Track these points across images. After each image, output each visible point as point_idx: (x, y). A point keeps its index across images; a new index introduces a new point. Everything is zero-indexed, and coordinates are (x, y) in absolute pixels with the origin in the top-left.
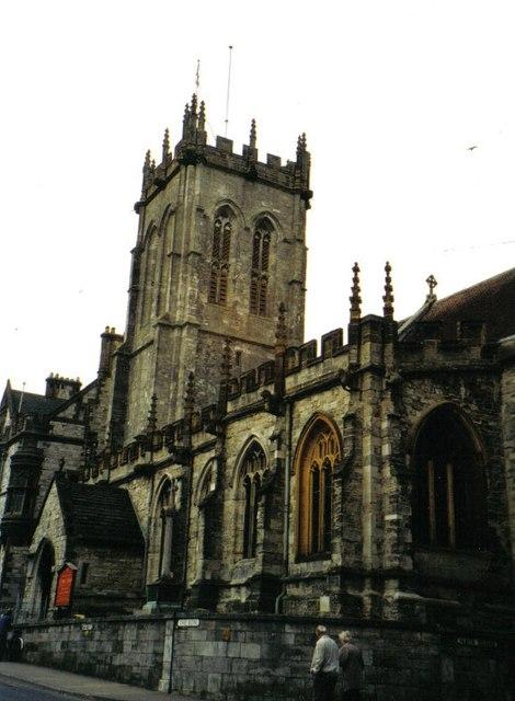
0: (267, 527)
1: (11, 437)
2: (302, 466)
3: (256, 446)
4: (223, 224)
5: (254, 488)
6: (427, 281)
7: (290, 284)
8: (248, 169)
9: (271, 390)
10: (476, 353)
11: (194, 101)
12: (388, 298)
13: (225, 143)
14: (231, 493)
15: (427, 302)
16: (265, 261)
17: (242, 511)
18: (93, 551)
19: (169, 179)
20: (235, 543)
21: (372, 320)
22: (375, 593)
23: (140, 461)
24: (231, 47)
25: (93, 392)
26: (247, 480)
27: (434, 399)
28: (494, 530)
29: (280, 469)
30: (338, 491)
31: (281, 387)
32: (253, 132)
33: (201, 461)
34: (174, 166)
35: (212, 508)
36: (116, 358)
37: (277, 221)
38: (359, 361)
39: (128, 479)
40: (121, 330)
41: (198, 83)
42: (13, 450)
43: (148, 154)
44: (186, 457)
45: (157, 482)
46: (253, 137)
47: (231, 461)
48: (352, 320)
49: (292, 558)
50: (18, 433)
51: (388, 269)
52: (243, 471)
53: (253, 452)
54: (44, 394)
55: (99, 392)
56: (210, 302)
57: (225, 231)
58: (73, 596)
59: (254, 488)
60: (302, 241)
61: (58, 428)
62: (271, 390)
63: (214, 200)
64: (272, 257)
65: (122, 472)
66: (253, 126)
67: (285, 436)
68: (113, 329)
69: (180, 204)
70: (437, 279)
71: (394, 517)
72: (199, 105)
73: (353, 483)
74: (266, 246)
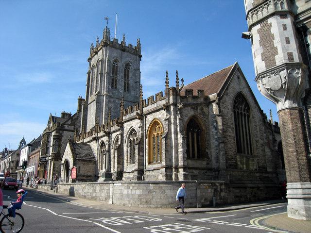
0: (139, 155)
3: (133, 130)
8: (123, 48)
9: (139, 112)
13: (116, 40)
14: (125, 145)
19: (99, 51)
23: (94, 136)
24: (106, 19)
26: (131, 141)
27: (192, 113)
28: (207, 153)
33: (114, 136)
34: (100, 47)
35: (120, 149)
38: (169, 102)
39: (90, 141)
40: (84, 97)
42: (53, 134)
44: (109, 134)
45: (99, 142)
46: (124, 39)
47: (125, 135)
51: (177, 73)
52: (129, 137)
53: (132, 132)
58: (77, 176)
61: (66, 127)
62: (139, 112)
64: (131, 75)
74: (128, 71)
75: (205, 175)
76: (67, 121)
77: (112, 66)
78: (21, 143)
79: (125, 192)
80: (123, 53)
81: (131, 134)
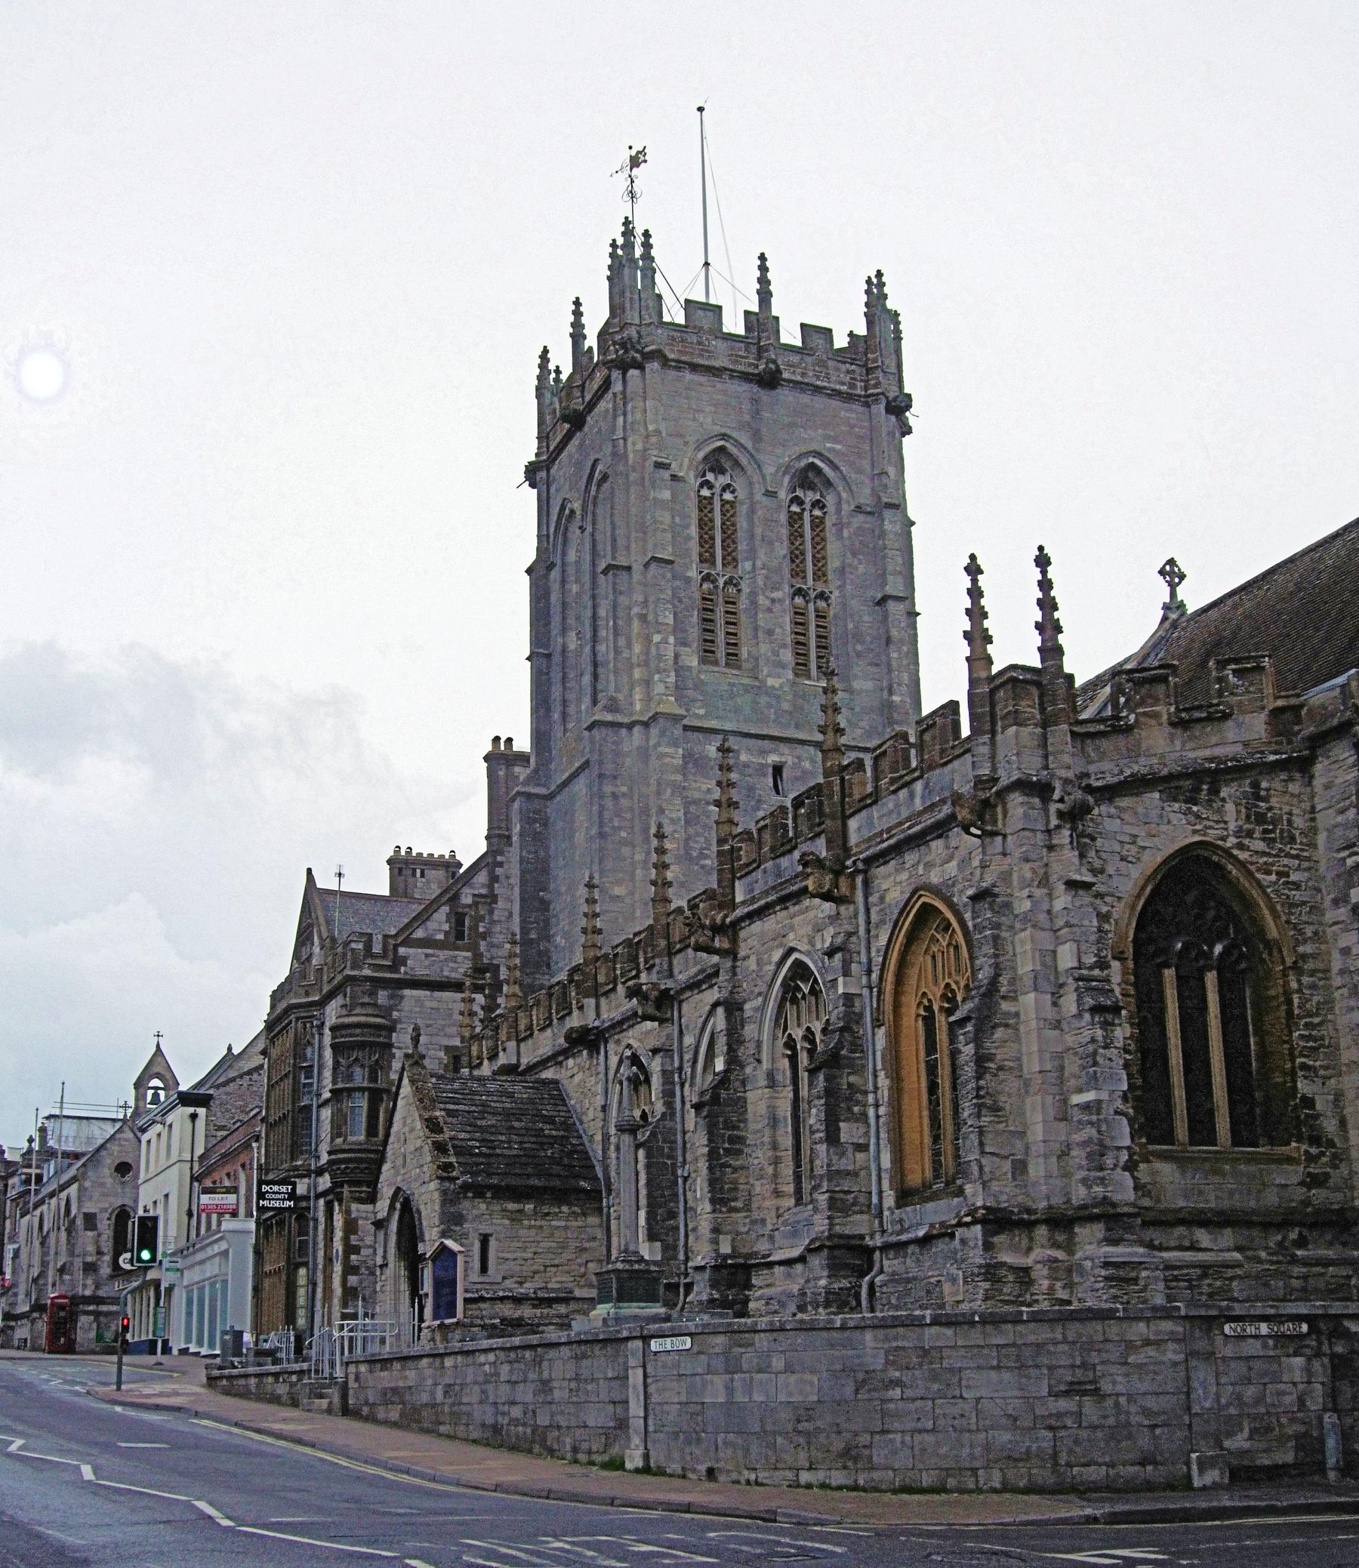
0: (832, 1138)
1: (326, 989)
2: (897, 1006)
3: (800, 971)
4: (717, 490)
5: (803, 1059)
6: (1162, 572)
7: (882, 601)
9: (820, 848)
10: (1256, 726)
11: (628, 231)
12: (1049, 627)
13: (701, 312)
15: (1165, 619)
16: (819, 560)
17: (785, 1108)
18: (497, 1208)
19: (591, 406)
20: (776, 1175)
21: (1016, 679)
22: (1060, 1255)
23: (575, 1021)
24: (701, 109)
25: (482, 878)
28: (1308, 1102)
29: (851, 1020)
30: (968, 1050)
31: (840, 841)
32: (764, 281)
36: (516, 805)
37: (835, 467)
39: (555, 1059)
41: (632, 195)
43: (544, 355)
46: (765, 295)
48: (973, 682)
49: (889, 1200)
50: (339, 978)
51: (1042, 561)
54: (385, 891)
55: (494, 879)
56: (703, 661)
57: (724, 503)
59: (803, 1059)
60: (898, 506)
61: (417, 962)
62: (820, 848)
63: (691, 439)
65: (546, 1043)
66: (763, 269)
67: (858, 944)
68: (509, 740)
69: (618, 456)
70: (1183, 565)
71: (1090, 1096)
72: (639, 240)
73: (999, 1033)
74: (818, 524)
75: (1294, 1260)
76: (421, 918)
77: (692, 506)
78: (140, 1085)
79: (715, 1392)
80: (764, 395)
81: (790, 994)
